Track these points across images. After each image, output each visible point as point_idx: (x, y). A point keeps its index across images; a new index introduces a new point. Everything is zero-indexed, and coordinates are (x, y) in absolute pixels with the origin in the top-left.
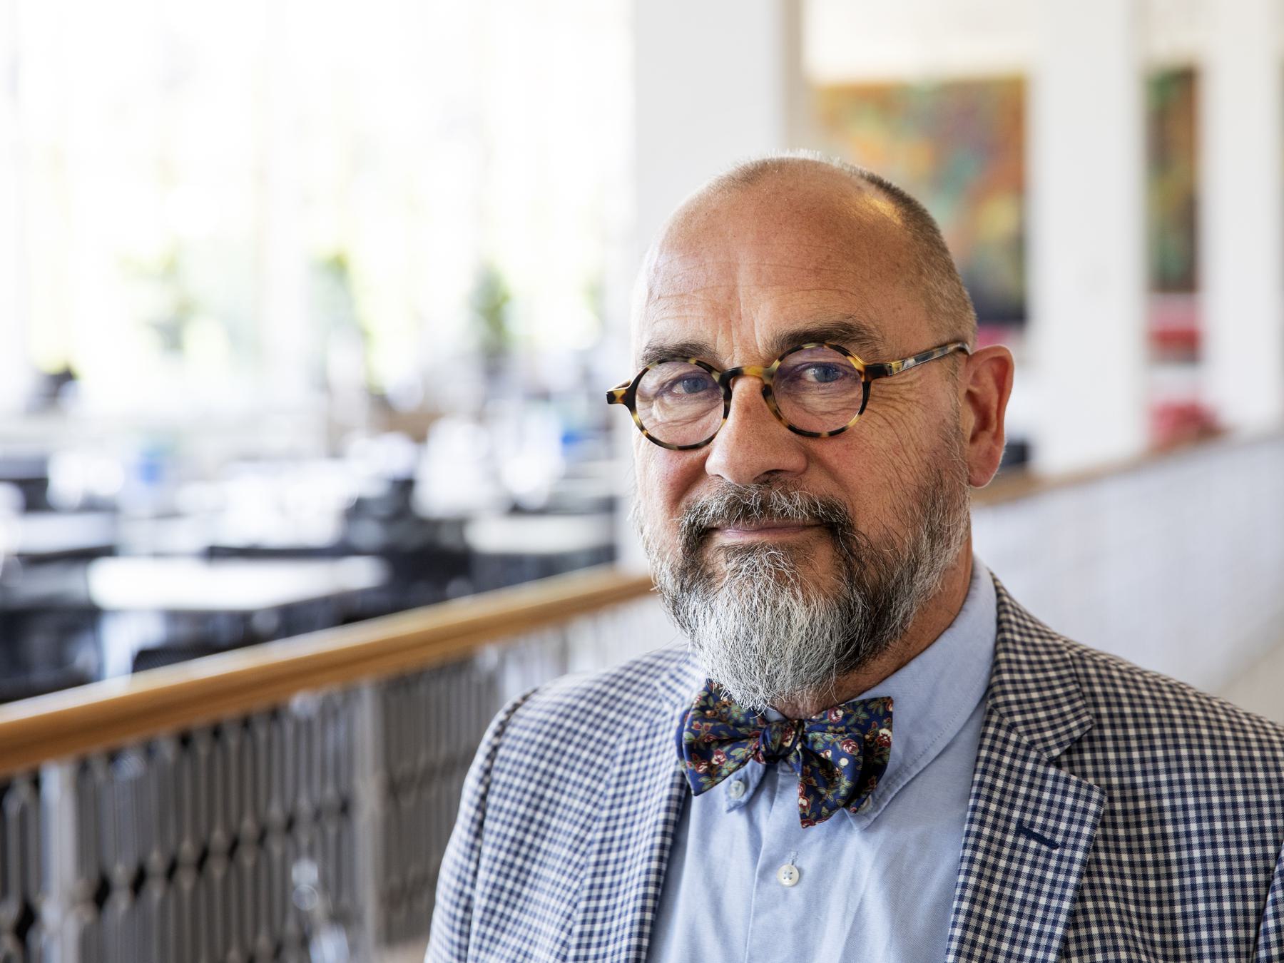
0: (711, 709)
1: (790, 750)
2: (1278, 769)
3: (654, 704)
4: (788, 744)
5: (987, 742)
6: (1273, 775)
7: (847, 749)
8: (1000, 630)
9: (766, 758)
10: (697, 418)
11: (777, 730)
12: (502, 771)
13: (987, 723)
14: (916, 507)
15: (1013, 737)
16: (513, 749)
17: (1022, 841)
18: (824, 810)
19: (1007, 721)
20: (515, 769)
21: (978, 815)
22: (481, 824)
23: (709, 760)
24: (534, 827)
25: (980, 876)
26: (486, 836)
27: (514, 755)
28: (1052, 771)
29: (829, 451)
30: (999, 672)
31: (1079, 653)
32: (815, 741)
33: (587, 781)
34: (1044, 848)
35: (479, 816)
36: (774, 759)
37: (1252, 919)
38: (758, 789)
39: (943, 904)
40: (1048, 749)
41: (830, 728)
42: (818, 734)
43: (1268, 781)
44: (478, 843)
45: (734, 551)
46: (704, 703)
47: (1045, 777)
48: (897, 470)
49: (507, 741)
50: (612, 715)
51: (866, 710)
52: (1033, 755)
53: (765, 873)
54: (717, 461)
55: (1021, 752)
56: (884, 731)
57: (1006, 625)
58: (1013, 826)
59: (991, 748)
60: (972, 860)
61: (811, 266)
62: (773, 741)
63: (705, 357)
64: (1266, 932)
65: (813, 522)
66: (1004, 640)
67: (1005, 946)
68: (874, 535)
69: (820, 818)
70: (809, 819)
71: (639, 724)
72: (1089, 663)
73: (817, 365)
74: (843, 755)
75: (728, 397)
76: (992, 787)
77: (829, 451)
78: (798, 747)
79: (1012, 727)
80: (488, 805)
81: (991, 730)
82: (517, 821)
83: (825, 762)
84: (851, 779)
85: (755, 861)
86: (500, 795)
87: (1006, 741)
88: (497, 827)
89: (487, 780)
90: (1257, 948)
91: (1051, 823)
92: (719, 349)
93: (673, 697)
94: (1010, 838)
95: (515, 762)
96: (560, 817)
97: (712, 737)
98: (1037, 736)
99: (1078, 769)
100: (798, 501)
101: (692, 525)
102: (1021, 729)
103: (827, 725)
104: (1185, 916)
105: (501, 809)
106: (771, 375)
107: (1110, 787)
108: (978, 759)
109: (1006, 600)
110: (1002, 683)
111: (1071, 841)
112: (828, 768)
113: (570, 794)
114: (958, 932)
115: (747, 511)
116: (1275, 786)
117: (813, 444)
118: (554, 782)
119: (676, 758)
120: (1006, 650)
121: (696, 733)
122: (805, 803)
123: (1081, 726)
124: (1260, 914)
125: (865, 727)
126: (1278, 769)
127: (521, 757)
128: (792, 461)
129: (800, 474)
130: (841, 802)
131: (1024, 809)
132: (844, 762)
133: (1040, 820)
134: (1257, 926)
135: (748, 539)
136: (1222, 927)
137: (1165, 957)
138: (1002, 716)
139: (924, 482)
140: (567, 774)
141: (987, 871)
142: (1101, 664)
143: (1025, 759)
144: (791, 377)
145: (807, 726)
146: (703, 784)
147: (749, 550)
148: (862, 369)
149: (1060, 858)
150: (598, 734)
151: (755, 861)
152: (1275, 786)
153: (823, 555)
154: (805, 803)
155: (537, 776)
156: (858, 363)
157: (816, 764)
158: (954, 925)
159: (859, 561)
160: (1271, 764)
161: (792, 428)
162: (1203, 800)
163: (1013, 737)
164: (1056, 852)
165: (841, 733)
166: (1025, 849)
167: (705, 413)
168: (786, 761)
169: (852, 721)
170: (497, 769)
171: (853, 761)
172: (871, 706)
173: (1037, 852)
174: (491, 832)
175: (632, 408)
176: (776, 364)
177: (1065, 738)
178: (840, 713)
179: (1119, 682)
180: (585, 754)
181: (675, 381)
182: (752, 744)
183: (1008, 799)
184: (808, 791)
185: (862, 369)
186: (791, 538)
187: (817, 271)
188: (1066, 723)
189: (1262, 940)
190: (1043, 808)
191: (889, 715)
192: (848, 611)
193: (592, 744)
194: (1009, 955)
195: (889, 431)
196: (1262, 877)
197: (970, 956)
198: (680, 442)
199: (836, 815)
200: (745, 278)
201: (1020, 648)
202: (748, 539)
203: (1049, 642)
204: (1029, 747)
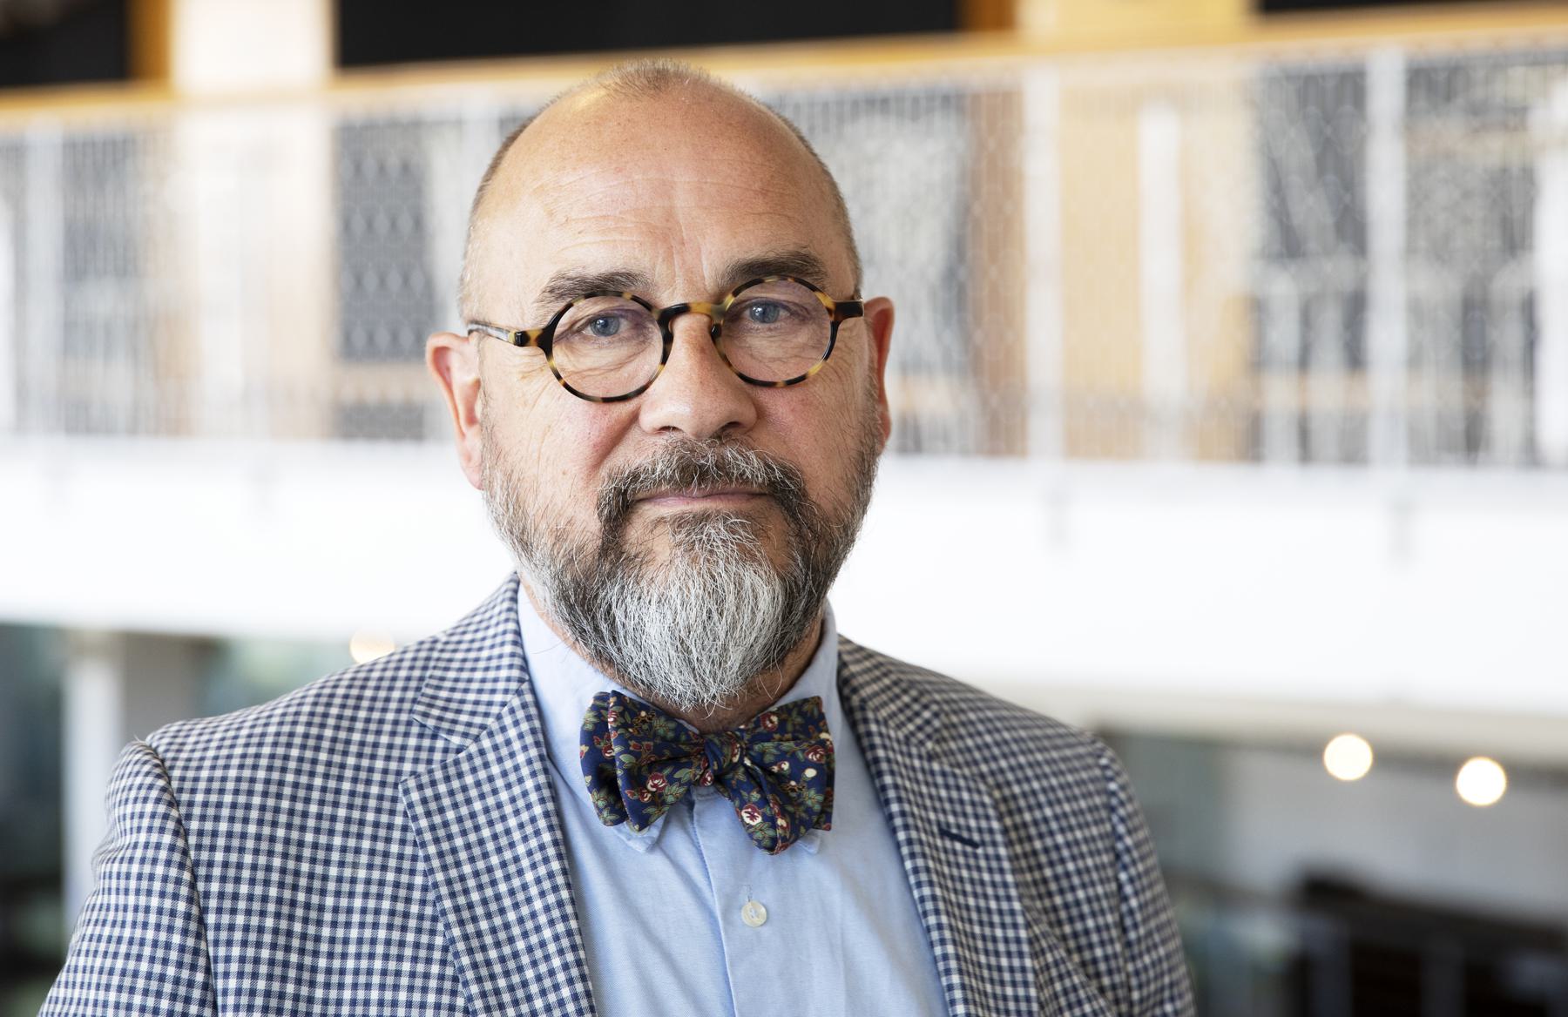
10: (621, 365)
45: (680, 522)
51: (801, 713)
61: (757, 186)
63: (637, 289)
67: (402, 996)
68: (827, 506)
75: (668, 339)
92: (656, 279)
106: (723, 314)
115: (703, 475)
117: (764, 396)
135: (698, 507)
137: (998, 1011)
144: (734, 316)
146: (649, 816)
147: (704, 518)
148: (831, 306)
153: (776, 523)
156: (828, 302)
162: (291, 864)
167: (630, 358)
172: (806, 708)
175: (548, 353)
176: (730, 300)
181: (592, 321)
183: (321, 855)
185: (831, 306)
187: (764, 192)
194: (143, 1009)
197: (280, 1011)
198: (601, 394)
200: (684, 202)
202: (698, 507)
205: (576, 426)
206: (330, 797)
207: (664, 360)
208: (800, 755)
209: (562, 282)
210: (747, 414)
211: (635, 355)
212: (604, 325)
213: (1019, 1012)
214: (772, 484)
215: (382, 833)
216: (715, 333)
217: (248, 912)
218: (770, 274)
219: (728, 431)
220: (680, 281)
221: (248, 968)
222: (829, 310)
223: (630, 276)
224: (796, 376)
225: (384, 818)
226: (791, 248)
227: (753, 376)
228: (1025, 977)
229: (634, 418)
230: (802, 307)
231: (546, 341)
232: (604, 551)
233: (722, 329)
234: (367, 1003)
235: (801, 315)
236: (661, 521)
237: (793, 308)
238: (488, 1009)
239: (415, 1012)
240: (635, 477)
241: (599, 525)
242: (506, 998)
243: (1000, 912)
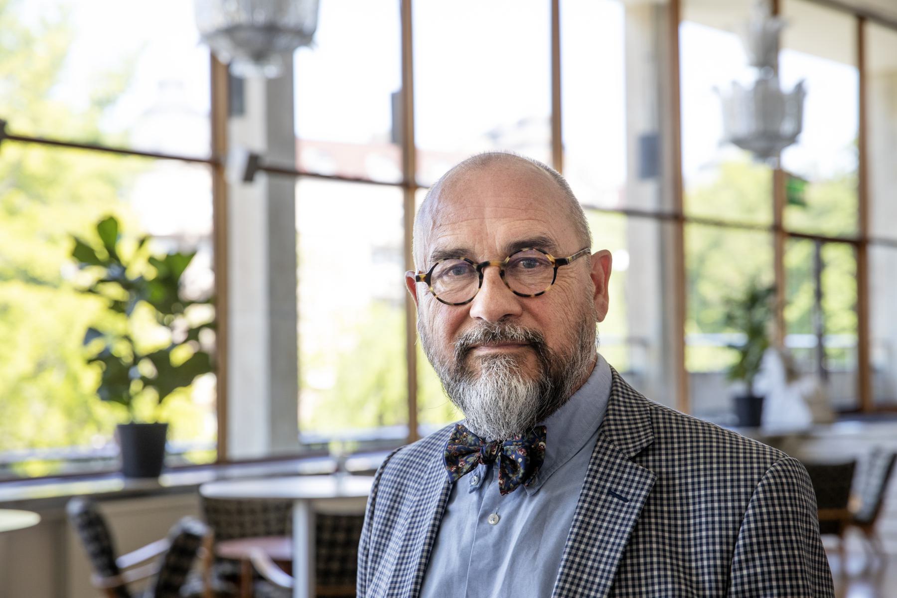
7: (521, 453)
8: (612, 394)
10: (463, 288)
14: (575, 333)
15: (611, 447)
19: (609, 439)
29: (533, 304)
30: (608, 415)
32: (507, 451)
34: (621, 502)
37: (731, 540)
39: (564, 531)
40: (629, 453)
45: (485, 358)
48: (566, 314)
52: (621, 455)
54: (478, 309)
55: (615, 454)
56: (542, 443)
57: (615, 392)
58: (606, 491)
61: (523, 207)
64: (738, 547)
65: (526, 343)
66: (613, 400)
68: (556, 348)
70: (505, 490)
73: (524, 259)
75: (481, 277)
77: (533, 304)
81: (600, 443)
84: (525, 469)
90: (733, 556)
92: (476, 251)
98: (624, 447)
99: (644, 464)
100: (519, 331)
101: (462, 345)
102: (616, 443)
104: (695, 539)
106: (504, 265)
107: (661, 473)
110: (608, 420)
111: (635, 498)
112: (514, 463)
114: (570, 543)
115: (494, 337)
117: (526, 301)
120: (613, 405)
123: (648, 441)
124: (735, 538)
125: (532, 441)
128: (515, 308)
129: (518, 316)
132: (520, 460)
133: (620, 488)
134: (734, 544)
136: (714, 544)
138: (606, 436)
139: (579, 320)
141: (589, 513)
143: (616, 457)
144: (513, 265)
147: (495, 356)
149: (629, 507)
151: (479, 509)
153: (531, 359)
156: (551, 258)
157: (508, 462)
158: (569, 540)
159: (549, 361)
161: (515, 292)
164: (627, 504)
166: (611, 502)
167: (468, 285)
171: (525, 460)
176: (508, 259)
181: (451, 269)
182: (477, 454)
186: (514, 350)
189: (736, 552)
191: (545, 434)
192: (542, 388)
195: (564, 294)
196: (737, 518)
198: (454, 302)
199: (519, 488)
204: (618, 452)
206: (695, 461)
212: (457, 270)
213: (698, 595)
214: (528, 340)
217: (707, 530)
218: (526, 247)
221: (581, 568)
228: (796, 575)
229: (468, 312)
231: (428, 279)
233: (507, 270)
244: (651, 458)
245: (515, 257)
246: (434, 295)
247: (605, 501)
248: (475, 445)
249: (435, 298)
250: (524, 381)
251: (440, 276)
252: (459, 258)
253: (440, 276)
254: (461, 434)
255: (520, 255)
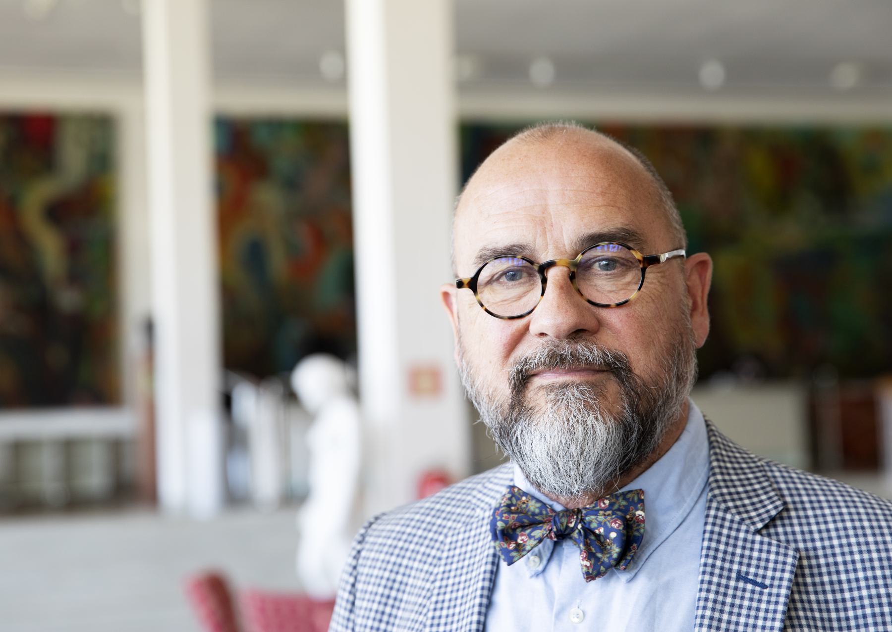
0: (515, 506)
1: (573, 530)
2: (887, 550)
3: (468, 512)
4: (572, 525)
5: (711, 520)
6: (884, 555)
7: (615, 526)
9: (557, 536)
10: (520, 297)
11: (563, 516)
12: (365, 566)
13: (709, 508)
16: (371, 550)
17: (741, 585)
18: (602, 568)
19: (723, 506)
20: (368, 579)
21: (709, 569)
22: (353, 604)
23: (516, 541)
24: (391, 602)
25: (713, 609)
26: (357, 611)
27: (372, 555)
28: (758, 538)
31: (767, 463)
32: (590, 522)
33: (426, 567)
34: (758, 589)
35: (351, 598)
36: (563, 536)
38: (549, 560)
40: (754, 523)
41: (601, 512)
42: (593, 517)
43: (880, 559)
44: (352, 617)
45: (551, 388)
46: (509, 502)
47: (753, 542)
49: (367, 546)
50: (439, 521)
51: (625, 499)
52: (744, 527)
53: (558, 616)
55: (735, 526)
56: (639, 513)
57: (715, 444)
58: (734, 575)
59: (714, 524)
60: (706, 599)
61: (598, 191)
62: (562, 524)
63: (527, 253)
67: (743, 620)
68: (646, 377)
69: (599, 574)
71: (460, 525)
72: (774, 469)
74: (613, 530)
75: (544, 281)
76: (717, 550)
78: (580, 526)
79: (727, 509)
80: (357, 590)
81: (712, 512)
82: (378, 598)
83: (598, 536)
85: (552, 609)
86: (364, 582)
87: (724, 519)
88: (365, 604)
89: (355, 573)
91: (761, 572)
92: (537, 247)
93: (482, 505)
94: (732, 583)
95: (373, 559)
96: (409, 593)
97: (518, 524)
103: (598, 510)
105: (366, 592)
108: (704, 532)
109: (713, 428)
111: (776, 583)
113: (415, 577)
115: (562, 359)
116: (886, 563)
117: (604, 313)
118: (402, 570)
119: (490, 538)
121: (506, 522)
122: (588, 564)
126: (887, 550)
127: (377, 556)
130: (613, 562)
131: (741, 563)
132: (613, 535)
133: (752, 570)
140: (411, 563)
141: (718, 606)
142: (783, 469)
143: (738, 530)
145: (584, 512)
146: (513, 557)
147: (565, 386)
148: (641, 258)
149: (770, 595)
150: (431, 535)
152: (886, 563)
153: (612, 386)
154: (588, 564)
155: (390, 567)
156: (638, 256)
157: (593, 537)
160: (881, 547)
163: (729, 516)
164: (766, 591)
165: (609, 515)
166: (744, 590)
168: (571, 538)
169: (616, 507)
170: (362, 565)
173: (753, 592)
174: (361, 608)
177: (765, 516)
178: (607, 502)
179: (797, 480)
180: (423, 549)
181: (505, 273)
182: (547, 527)
184: (590, 556)
185: (641, 258)
187: (603, 194)
188: (764, 506)
190: (754, 562)
192: (626, 429)
193: (426, 542)
200: (553, 201)
201: (726, 459)
203: (745, 456)
204: (740, 523)
205: (497, 333)
207: (542, 295)
208: (608, 524)
209: (484, 252)
210: (590, 323)
211: (528, 292)
212: (513, 275)
214: (608, 364)
215: (732, 541)
216: (572, 277)
219: (576, 334)
220: (551, 247)
222: (639, 261)
223: (522, 247)
224: (623, 300)
225: (733, 533)
226: (619, 226)
227: (597, 301)
229: (527, 328)
230: (627, 260)
231: (473, 284)
232: (512, 407)
234: (737, 624)
235: (626, 265)
236: (542, 387)
237: (621, 261)
238: (840, 629)
239: (749, 630)
240: (526, 362)
241: (509, 391)
242: (870, 620)
243: (822, 620)
244: (780, 530)
245: (589, 255)
246: (482, 305)
247: (736, 588)
248: (541, 514)
249: (482, 310)
250: (603, 418)
251: (489, 282)
252: (514, 256)
253: (489, 282)
254: (518, 499)
255: (598, 252)
